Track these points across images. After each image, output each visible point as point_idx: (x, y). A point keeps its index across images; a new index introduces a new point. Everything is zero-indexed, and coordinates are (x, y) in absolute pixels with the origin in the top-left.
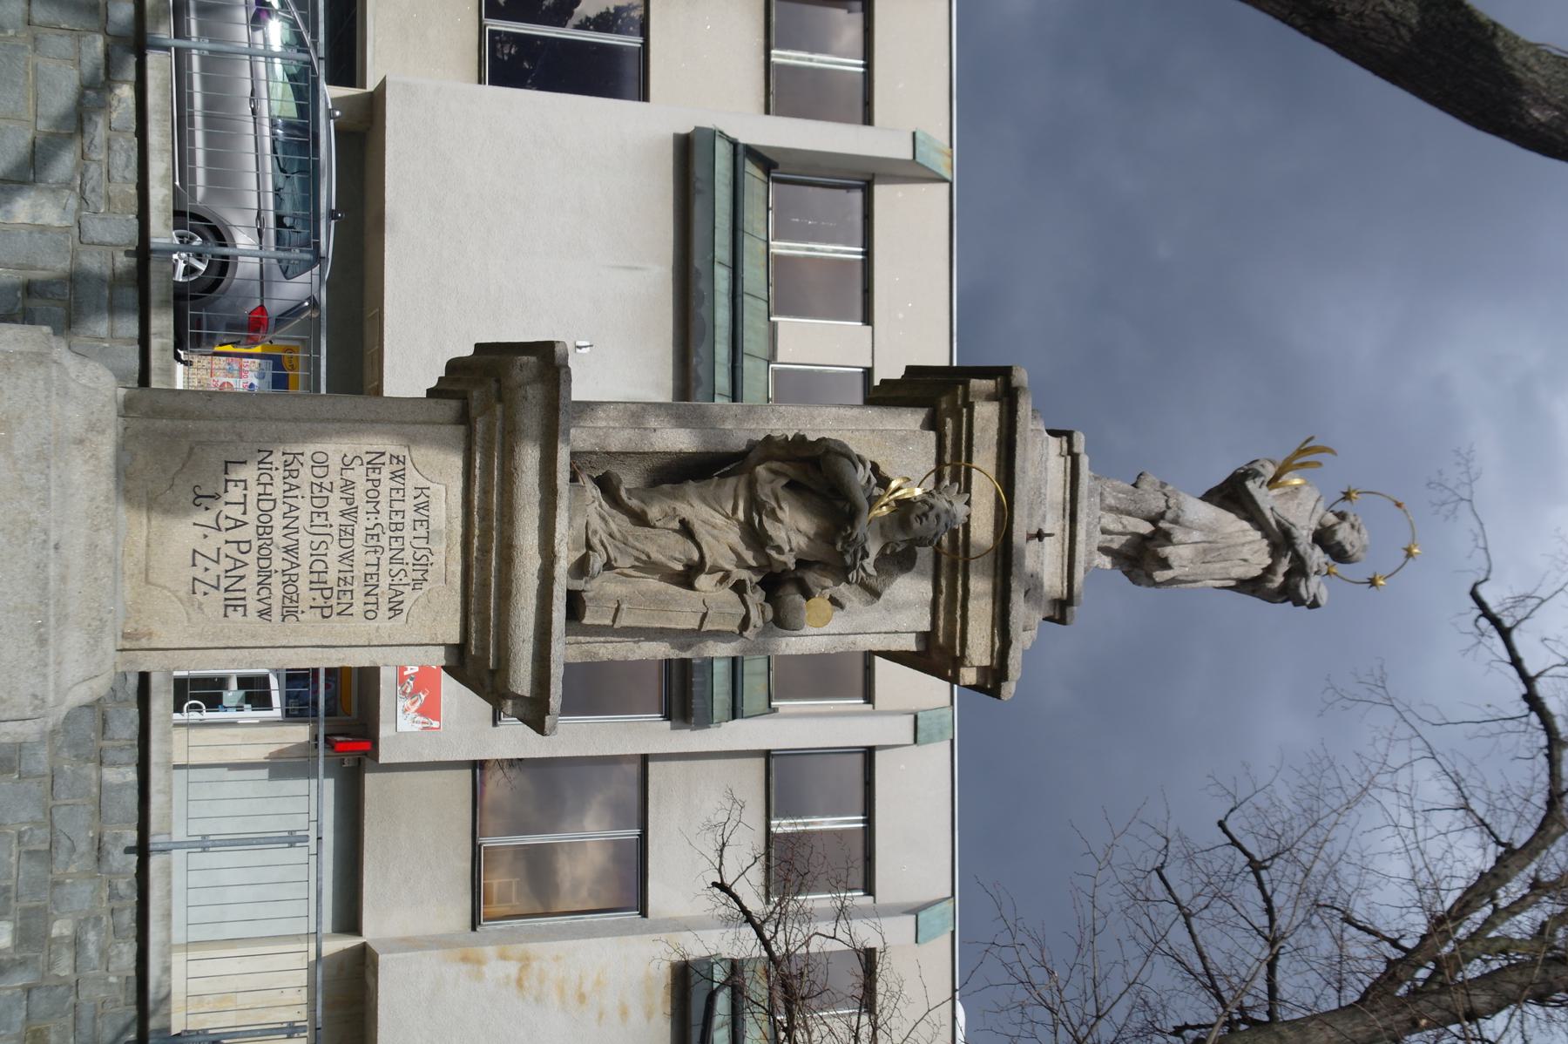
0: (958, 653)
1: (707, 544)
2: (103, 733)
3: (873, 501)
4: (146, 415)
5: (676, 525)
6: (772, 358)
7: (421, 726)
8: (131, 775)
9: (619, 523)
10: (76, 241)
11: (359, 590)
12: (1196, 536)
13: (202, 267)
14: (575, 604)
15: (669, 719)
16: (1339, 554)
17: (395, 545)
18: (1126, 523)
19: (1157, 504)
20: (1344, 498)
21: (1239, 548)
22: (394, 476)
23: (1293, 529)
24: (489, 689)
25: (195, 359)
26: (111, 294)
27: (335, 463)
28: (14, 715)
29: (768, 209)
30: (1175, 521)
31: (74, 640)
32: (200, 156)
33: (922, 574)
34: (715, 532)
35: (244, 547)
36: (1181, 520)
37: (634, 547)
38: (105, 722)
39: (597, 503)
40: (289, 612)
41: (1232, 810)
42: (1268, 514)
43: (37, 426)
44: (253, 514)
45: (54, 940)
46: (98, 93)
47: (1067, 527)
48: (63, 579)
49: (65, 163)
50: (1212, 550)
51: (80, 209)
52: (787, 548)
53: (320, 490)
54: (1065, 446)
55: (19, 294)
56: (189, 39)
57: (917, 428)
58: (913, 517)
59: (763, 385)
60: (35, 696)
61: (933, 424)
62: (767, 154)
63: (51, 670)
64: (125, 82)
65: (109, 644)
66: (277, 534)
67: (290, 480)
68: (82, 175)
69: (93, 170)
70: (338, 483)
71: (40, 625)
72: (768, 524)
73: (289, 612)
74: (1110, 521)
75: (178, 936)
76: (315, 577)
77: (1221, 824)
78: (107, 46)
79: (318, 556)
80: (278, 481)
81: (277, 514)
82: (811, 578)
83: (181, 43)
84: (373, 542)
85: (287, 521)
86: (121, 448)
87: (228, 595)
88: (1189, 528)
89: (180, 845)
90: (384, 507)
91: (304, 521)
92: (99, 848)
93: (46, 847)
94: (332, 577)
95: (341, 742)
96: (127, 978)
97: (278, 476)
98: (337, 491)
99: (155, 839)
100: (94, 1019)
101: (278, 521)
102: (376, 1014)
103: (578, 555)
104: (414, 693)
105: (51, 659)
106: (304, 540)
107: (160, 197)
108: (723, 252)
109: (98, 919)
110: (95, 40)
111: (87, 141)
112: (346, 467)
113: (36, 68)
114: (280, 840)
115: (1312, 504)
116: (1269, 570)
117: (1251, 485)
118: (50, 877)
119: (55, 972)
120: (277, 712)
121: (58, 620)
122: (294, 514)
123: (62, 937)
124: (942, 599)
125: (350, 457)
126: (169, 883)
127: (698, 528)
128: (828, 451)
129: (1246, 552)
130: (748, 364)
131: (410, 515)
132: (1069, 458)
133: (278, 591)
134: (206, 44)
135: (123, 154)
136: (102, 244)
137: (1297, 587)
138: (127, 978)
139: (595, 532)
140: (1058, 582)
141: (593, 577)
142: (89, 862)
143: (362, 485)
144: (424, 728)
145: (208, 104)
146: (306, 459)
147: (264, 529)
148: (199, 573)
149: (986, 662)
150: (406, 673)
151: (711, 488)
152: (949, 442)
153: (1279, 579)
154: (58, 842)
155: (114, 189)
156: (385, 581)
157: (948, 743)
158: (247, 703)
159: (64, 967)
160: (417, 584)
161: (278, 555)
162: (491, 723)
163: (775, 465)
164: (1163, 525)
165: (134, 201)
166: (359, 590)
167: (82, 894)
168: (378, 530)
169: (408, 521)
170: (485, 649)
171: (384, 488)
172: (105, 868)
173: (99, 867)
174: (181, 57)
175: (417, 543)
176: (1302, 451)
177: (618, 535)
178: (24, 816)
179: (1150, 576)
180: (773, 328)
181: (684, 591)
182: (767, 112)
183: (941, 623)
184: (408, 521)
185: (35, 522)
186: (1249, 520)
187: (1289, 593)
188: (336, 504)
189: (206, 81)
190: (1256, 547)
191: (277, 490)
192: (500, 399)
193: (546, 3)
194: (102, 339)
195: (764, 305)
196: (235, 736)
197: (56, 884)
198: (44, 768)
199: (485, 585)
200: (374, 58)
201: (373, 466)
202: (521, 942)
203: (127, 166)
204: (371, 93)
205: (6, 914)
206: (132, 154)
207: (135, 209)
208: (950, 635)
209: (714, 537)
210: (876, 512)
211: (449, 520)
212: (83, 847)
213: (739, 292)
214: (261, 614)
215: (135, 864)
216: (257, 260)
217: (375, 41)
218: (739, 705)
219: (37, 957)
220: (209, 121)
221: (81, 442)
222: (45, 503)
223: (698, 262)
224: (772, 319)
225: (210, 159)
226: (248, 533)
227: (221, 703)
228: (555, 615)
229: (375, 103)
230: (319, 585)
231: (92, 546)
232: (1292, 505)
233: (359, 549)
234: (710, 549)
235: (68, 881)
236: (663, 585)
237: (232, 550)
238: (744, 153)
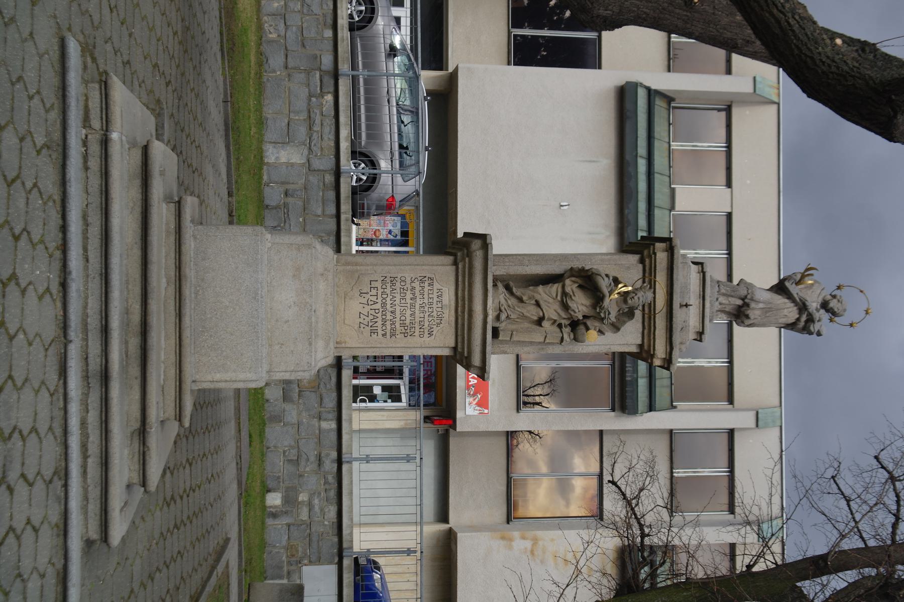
0: (652, 353)
1: (546, 309)
2: (321, 405)
3: (611, 293)
4: (343, 265)
5: (533, 302)
6: (672, 208)
7: (478, 412)
8: (333, 425)
9: (513, 301)
10: (307, 169)
11: (417, 326)
12: (761, 305)
13: (364, 178)
14: (496, 333)
15: (614, 411)
16: (833, 313)
17: (430, 310)
18: (730, 300)
20: (837, 289)
21: (782, 311)
22: (429, 285)
23: (806, 302)
24: (465, 364)
25: (360, 222)
26: (323, 194)
27: (408, 280)
28: (302, 369)
29: (670, 124)
30: (752, 299)
31: (320, 344)
34: (549, 305)
35: (377, 311)
36: (754, 298)
37: (518, 311)
38: (321, 399)
39: (503, 294)
40: (393, 335)
41: (882, 450)
42: (795, 296)
43: (308, 270)
44: (379, 300)
45: (299, 503)
46: (317, 99)
47: (701, 302)
48: (317, 322)
50: (770, 311)
51: (309, 154)
52: (577, 311)
53: (403, 290)
54: (700, 269)
55: (282, 196)
56: (358, 71)
57: (635, 263)
58: (628, 298)
59: (667, 224)
60: (308, 363)
61: (642, 261)
62: (668, 94)
63: (313, 354)
65: (332, 345)
66: (388, 306)
67: (393, 287)
69: (315, 136)
70: (410, 288)
71: (309, 339)
72: (569, 302)
73: (393, 335)
74: (722, 299)
75: (356, 519)
76: (402, 322)
77: (876, 458)
78: (321, 76)
79: (403, 315)
80: (388, 287)
81: (388, 299)
82: (589, 323)
83: (355, 73)
84: (422, 309)
85: (392, 302)
87: (372, 328)
88: (758, 302)
89: (356, 459)
90: (426, 296)
91: (398, 302)
92: (319, 460)
93: (296, 458)
94: (408, 322)
95: (437, 420)
96: (333, 522)
97: (389, 285)
98: (409, 291)
99: (345, 457)
100: (318, 542)
101: (389, 302)
102: (457, 565)
103: (496, 313)
104: (474, 395)
105: (313, 350)
106: (398, 308)
107: (345, 147)
108: (642, 150)
109: (320, 494)
110: (315, 74)
112: (412, 282)
113: (289, 89)
114: (402, 459)
115: (819, 291)
116: (798, 319)
117: (787, 284)
118: (298, 473)
119: (300, 518)
120: (404, 403)
121: (315, 337)
122: (394, 299)
123: (303, 501)
125: (414, 278)
126: (351, 478)
127: (542, 303)
128: (593, 273)
129: (785, 312)
130: (657, 212)
131: (435, 299)
132: (702, 274)
133: (389, 327)
134: (366, 73)
135: (328, 127)
136: (318, 170)
137: (809, 327)
138: (333, 522)
139: (502, 305)
140: (697, 324)
141: (502, 322)
142: (314, 466)
143: (418, 289)
144: (480, 413)
146: (398, 279)
147: (384, 305)
149: (664, 356)
150: (470, 384)
151: (548, 288)
152: (647, 268)
154: (301, 456)
156: (426, 324)
157: (778, 429)
158: (389, 398)
159: (304, 515)
160: (438, 324)
161: (389, 314)
162: (515, 411)
163: (573, 279)
164: (746, 301)
166: (417, 326)
167: (313, 482)
168: (424, 305)
169: (435, 301)
170: (463, 348)
171: (426, 290)
172: (322, 469)
173: (320, 469)
174: (355, 80)
175: (438, 309)
176: (807, 270)
177: (511, 306)
178: (286, 443)
179: (743, 322)
180: (673, 191)
181: (538, 327)
182: (669, 71)
183: (646, 341)
184: (435, 301)
185: (308, 303)
186: (788, 298)
187: (806, 330)
188: (409, 295)
190: (790, 310)
191: (388, 291)
192: (468, 256)
193: (552, 3)
194: (319, 216)
195: (667, 179)
196: (383, 416)
197: (301, 476)
198: (295, 421)
200: (452, 52)
201: (422, 281)
202: (532, 530)
203: (330, 133)
204: (451, 73)
205: (279, 489)
206: (332, 127)
207: (334, 153)
208: (649, 346)
209: (548, 306)
210: (612, 297)
211: (450, 301)
212: (312, 458)
213: (652, 171)
214: (383, 335)
215: (336, 468)
216: (390, 175)
217: (453, 45)
218: (653, 403)
219: (292, 511)
221: (322, 275)
223: (628, 157)
224: (672, 186)
225: (368, 118)
226: (378, 306)
227: (376, 398)
228: (487, 336)
229: (453, 79)
230: (403, 325)
231: (326, 311)
232: (809, 292)
233: (417, 312)
234: (547, 311)
235: (306, 475)
236: (530, 325)
237: (372, 312)
238: (652, 94)
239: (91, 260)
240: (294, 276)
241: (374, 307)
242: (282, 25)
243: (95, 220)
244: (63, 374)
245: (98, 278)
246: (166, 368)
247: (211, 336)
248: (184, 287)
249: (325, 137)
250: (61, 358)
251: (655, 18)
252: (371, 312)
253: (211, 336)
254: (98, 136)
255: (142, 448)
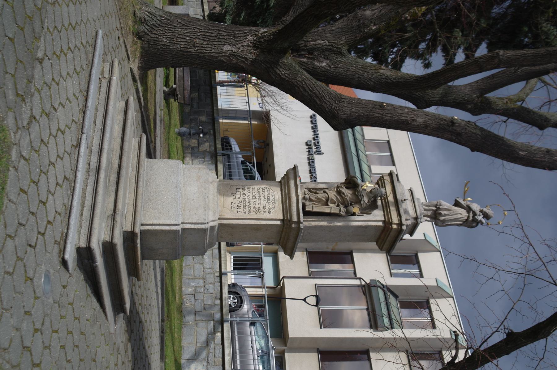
19: (435, 202)
22: (267, 191)
30: (440, 205)
32: (237, 347)
33: (380, 210)
44: (242, 197)
49: (204, 355)
51: (207, 365)
53: (254, 193)
64: (219, 332)
66: (246, 200)
68: (208, 356)
70: (257, 192)
73: (250, 212)
78: (214, 324)
80: (246, 191)
86: (218, 186)
90: (266, 196)
91: (251, 198)
94: (257, 207)
101: (246, 198)
106: (251, 201)
111: (209, 347)
112: (258, 189)
116: (468, 217)
124: (385, 213)
131: (271, 197)
133: (247, 209)
145: (240, 348)
147: (244, 199)
148: (233, 206)
149: (397, 222)
153: (471, 218)
155: (216, 359)
156: (267, 208)
160: (273, 208)
165: (221, 362)
183: (386, 217)
184: (271, 198)
188: (257, 195)
189: (239, 342)
191: (246, 193)
199: (286, 207)
207: (221, 364)
220: (240, 352)
222: (206, 189)
225: (241, 362)
230: (254, 208)
231: (214, 199)
239: (97, 124)
240: (197, 180)
241: (238, 200)
242: (193, 299)
243: (101, 110)
244: (78, 146)
245: (100, 131)
246: (128, 206)
247: (153, 203)
248: (140, 169)
249: (217, 356)
250: (78, 139)
251: (367, 115)
252: (237, 202)
253: (153, 203)
254: (107, 80)
255: (112, 223)
